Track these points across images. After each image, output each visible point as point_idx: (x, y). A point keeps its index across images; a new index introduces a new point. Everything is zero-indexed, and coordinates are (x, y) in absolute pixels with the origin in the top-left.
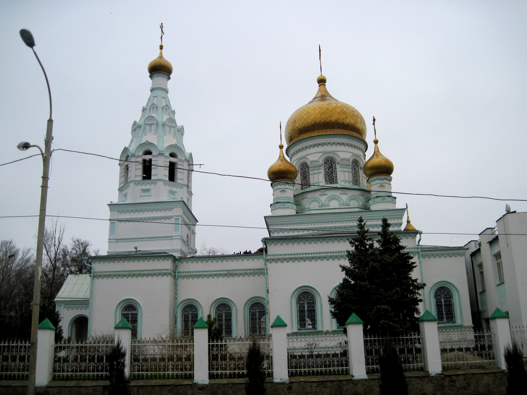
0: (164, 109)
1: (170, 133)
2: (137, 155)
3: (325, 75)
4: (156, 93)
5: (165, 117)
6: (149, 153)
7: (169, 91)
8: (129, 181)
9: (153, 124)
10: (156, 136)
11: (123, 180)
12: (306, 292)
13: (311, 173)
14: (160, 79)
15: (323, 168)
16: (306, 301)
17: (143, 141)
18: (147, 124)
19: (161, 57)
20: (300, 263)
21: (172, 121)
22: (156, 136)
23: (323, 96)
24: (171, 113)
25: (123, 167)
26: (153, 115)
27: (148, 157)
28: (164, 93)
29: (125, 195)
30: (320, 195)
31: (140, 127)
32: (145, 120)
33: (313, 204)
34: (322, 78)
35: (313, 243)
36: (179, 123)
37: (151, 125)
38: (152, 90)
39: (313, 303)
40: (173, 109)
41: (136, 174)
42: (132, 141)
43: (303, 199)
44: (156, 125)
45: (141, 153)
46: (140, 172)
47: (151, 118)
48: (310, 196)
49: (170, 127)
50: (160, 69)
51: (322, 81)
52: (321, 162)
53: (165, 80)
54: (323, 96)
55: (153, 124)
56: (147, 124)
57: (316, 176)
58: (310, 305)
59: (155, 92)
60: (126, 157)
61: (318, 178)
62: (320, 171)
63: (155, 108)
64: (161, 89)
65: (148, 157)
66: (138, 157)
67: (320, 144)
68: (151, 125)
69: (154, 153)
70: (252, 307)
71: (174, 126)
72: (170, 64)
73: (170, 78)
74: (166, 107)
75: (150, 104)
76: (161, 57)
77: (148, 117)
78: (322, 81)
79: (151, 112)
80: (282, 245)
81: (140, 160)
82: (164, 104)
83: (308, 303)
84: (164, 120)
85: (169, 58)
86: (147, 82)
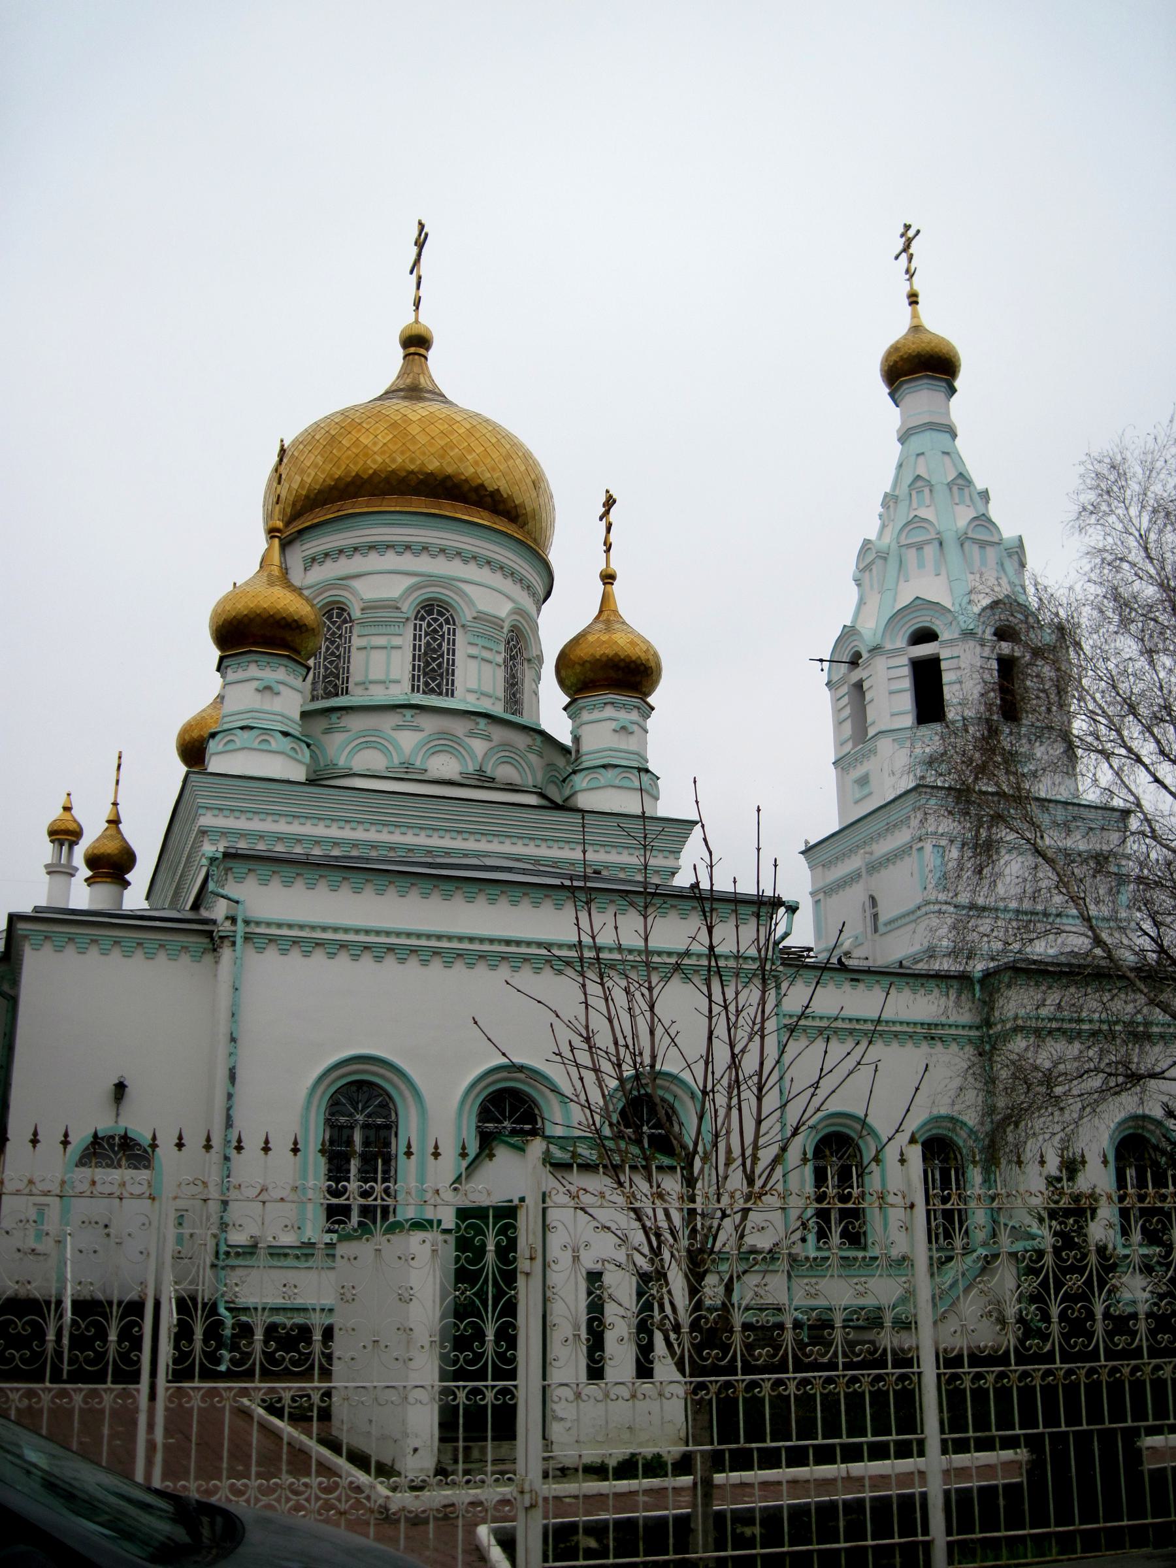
0: (955, 489)
1: (921, 565)
2: (888, 646)
3: (429, 321)
4: (916, 443)
5: (963, 517)
6: (925, 636)
7: (959, 432)
8: (870, 734)
9: (928, 542)
10: (943, 578)
11: (848, 728)
12: (360, 1084)
13: (356, 642)
14: (923, 396)
15: (409, 632)
16: (360, 1117)
17: (904, 600)
18: (909, 546)
19: (916, 328)
20: (888, 1049)
21: (983, 521)
22: (943, 578)
23: (413, 388)
24: (976, 498)
25: (845, 689)
26: (923, 513)
27: (924, 650)
28: (947, 436)
29: (863, 781)
30: (398, 728)
31: (883, 556)
32: (901, 530)
33: (358, 752)
34: (415, 331)
35: (322, 888)
36: (1008, 532)
37: (919, 547)
38: (904, 438)
39: (388, 1127)
40: (980, 485)
41: (895, 710)
42: (861, 602)
43: (328, 731)
44: (936, 543)
45: (901, 641)
46: (906, 702)
47: (917, 523)
48: (356, 723)
49: (983, 544)
50: (921, 367)
51: (416, 343)
52: (408, 607)
53: (940, 396)
54: (413, 388)
55: (928, 542)
56: (909, 546)
57: (377, 657)
58: (372, 1133)
59: (913, 439)
60: (850, 659)
61: (383, 665)
62: (397, 641)
63: (927, 490)
64: (933, 427)
65: (924, 650)
66: (896, 652)
67: (425, 549)
68: (919, 547)
69: (944, 635)
70: (335, 1106)
71: (996, 539)
72: (948, 343)
73: (953, 390)
74: (960, 481)
75: (908, 479)
76: (916, 328)
77: (908, 523)
78: (416, 343)
79: (915, 505)
80: (334, 889)
81: (904, 660)
82: (952, 475)
83: (366, 1126)
84: (962, 523)
85: (944, 324)
86: (882, 414)
